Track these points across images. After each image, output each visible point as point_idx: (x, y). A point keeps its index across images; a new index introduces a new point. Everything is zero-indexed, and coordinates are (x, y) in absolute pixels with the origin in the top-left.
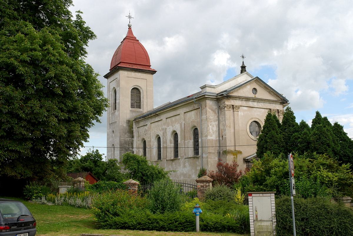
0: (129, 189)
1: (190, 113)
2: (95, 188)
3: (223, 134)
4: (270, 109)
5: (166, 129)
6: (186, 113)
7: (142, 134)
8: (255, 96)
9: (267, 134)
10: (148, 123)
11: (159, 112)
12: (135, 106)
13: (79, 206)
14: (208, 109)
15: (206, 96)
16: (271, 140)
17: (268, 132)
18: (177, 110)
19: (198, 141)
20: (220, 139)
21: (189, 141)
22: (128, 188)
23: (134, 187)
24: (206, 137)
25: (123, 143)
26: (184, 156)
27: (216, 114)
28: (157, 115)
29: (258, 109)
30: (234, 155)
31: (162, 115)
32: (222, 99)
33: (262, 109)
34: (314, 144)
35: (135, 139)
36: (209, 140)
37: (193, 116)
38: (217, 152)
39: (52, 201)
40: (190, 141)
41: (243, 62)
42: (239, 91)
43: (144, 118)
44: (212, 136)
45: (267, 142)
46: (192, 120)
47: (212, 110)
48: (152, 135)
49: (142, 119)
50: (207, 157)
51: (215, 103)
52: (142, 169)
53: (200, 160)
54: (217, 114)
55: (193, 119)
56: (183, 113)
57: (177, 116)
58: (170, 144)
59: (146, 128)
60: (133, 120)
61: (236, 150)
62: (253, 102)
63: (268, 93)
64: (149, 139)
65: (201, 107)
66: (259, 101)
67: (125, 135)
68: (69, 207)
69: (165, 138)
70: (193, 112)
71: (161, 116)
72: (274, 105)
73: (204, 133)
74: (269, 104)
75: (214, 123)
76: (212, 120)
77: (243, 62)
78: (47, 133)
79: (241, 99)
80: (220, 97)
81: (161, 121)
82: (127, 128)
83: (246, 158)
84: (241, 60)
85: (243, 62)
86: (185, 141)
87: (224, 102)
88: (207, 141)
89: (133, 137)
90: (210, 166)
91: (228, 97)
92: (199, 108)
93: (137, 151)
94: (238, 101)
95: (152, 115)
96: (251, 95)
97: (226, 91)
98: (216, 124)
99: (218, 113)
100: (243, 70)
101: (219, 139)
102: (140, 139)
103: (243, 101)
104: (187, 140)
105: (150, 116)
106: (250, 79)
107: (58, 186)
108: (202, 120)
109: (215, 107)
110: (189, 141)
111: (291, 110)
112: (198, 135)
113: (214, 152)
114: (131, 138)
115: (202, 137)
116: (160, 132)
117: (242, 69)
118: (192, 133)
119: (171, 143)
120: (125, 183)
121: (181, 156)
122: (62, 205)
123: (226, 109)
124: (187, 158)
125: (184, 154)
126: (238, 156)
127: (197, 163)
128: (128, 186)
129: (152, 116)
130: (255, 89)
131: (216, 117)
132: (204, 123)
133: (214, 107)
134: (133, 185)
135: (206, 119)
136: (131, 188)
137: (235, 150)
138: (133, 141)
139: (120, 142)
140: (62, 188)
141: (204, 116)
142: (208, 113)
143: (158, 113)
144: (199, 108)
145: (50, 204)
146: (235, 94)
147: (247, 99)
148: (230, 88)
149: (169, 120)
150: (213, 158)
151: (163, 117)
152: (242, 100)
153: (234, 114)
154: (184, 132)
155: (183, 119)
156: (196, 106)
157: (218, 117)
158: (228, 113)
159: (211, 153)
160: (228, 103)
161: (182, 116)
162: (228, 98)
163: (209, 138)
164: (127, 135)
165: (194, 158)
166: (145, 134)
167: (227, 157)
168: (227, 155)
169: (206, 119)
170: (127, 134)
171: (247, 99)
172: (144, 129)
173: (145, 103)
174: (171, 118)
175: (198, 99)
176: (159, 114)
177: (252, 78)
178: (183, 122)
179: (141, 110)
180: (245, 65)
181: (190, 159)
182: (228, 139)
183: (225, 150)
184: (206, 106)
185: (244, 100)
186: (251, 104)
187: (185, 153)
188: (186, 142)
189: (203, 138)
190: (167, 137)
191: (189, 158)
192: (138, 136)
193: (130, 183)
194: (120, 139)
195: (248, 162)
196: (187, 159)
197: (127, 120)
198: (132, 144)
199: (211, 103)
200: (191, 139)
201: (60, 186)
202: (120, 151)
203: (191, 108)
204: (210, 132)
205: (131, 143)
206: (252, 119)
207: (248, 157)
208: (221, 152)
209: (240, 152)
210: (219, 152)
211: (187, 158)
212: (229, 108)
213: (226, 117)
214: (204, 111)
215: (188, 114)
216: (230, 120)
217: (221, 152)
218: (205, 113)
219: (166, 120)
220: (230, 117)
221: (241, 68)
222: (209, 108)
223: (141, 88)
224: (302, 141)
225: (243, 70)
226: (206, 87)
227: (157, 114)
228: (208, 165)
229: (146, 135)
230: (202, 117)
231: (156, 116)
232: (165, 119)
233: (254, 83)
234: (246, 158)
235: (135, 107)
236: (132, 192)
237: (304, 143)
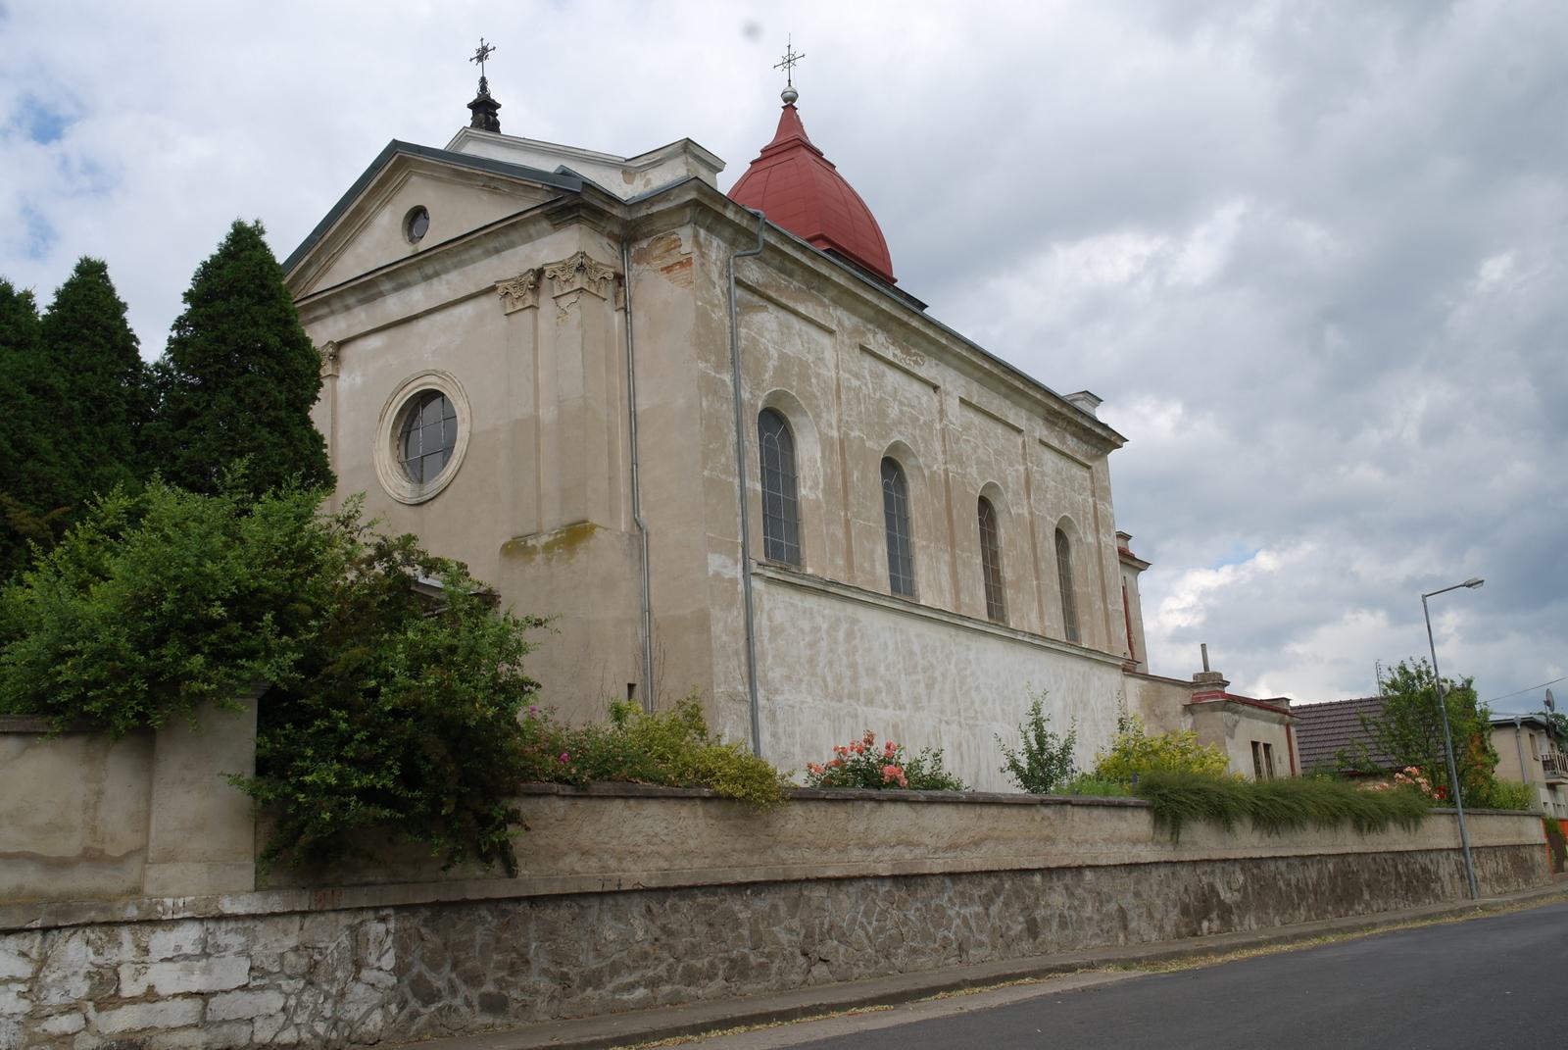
62: (404, 294)
74: (494, 260)
84: (782, 75)
85: (483, 81)
152: (348, 308)
185: (351, 300)
227: (753, 238)
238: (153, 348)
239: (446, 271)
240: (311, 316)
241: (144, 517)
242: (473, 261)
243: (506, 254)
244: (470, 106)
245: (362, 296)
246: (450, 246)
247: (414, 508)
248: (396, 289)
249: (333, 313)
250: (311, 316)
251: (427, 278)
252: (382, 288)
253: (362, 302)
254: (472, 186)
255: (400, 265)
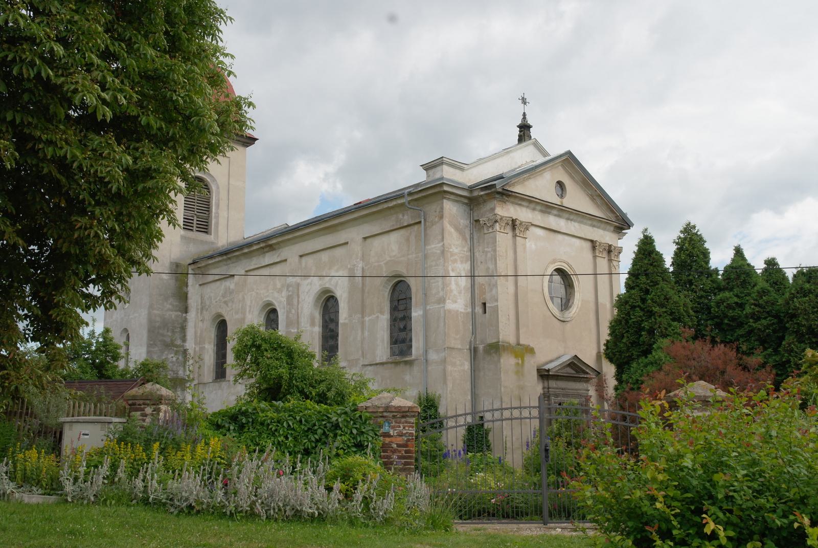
0: (382, 431)
1: (385, 239)
2: (232, 428)
3: (488, 296)
4: (592, 241)
5: (298, 285)
6: (369, 241)
7: (214, 302)
8: (562, 202)
9: (647, 292)
10: (238, 269)
11: (280, 239)
12: (195, 225)
13: (190, 507)
14: (448, 226)
15: (446, 188)
16: (664, 310)
17: (650, 286)
18: (338, 231)
19: (407, 318)
20: (476, 311)
21: (378, 317)
22: (381, 427)
23: (406, 422)
24: (439, 304)
25: (157, 324)
26: (361, 359)
27: (466, 241)
28: (271, 248)
29: (566, 238)
30: (516, 357)
31: (287, 248)
32: (485, 201)
33: (574, 240)
34: (807, 320)
35: (192, 316)
36: (450, 311)
37: (395, 247)
38: (468, 347)
39: (38, 483)
40: (381, 317)
41: (524, 113)
42: (526, 183)
43: (225, 257)
44: (456, 302)
45: (650, 314)
46: (388, 259)
47: (457, 229)
48: (248, 303)
49: (217, 260)
50: (444, 361)
51: (465, 211)
52: (304, 378)
53: (416, 369)
54: (469, 241)
55: (394, 254)
56: (359, 238)
57: (338, 248)
58: (309, 328)
59: (230, 284)
60: (190, 264)
61: (522, 342)
62: (557, 219)
63: (588, 199)
64: (239, 316)
65: (425, 220)
66: (572, 217)
67: (165, 304)
68: (145, 515)
69: (293, 311)
70: (394, 237)
71: (281, 250)
72: (601, 232)
73: (434, 291)
74: (590, 229)
75: (460, 266)
76: (456, 257)
77: (524, 113)
78: (44, 159)
79: (532, 206)
80: (482, 193)
81: (283, 264)
82: (172, 283)
83: (547, 363)
84: (520, 108)
85: (524, 114)
86: (363, 317)
87: (493, 209)
88: (442, 315)
89: (186, 310)
90: (450, 385)
91: (505, 195)
92: (420, 222)
93: (197, 349)
94: (524, 209)
95: (255, 247)
96: (551, 196)
97: (500, 177)
98: (466, 268)
99: (472, 238)
100: (524, 134)
101: (473, 313)
102: (208, 316)
103: (537, 213)
104: (369, 316)
105: (246, 250)
106: (541, 159)
107: (57, 417)
108: (426, 257)
109: (464, 222)
110: (378, 317)
111: (699, 233)
112: (411, 298)
113: (459, 347)
114: (180, 311)
115: (425, 302)
116: (276, 295)
117: (520, 131)
118: (387, 293)
119: (313, 324)
120: (366, 408)
121: (349, 361)
122: (100, 500)
123: (497, 226)
124: (371, 365)
125: (360, 352)
126: (525, 359)
127: (407, 378)
128: (380, 420)
129: (252, 249)
130: (560, 184)
131: (465, 249)
132: (434, 263)
133: (462, 221)
134: (403, 417)
135: (443, 252)
136: (393, 428)
137: (518, 344)
138: (185, 320)
139: (151, 321)
140: (75, 425)
141: (433, 246)
142: (446, 235)
143: (274, 241)
144: (420, 222)
145: (34, 498)
146: (518, 189)
147: (547, 207)
148: (510, 171)
149: (309, 261)
150: (458, 362)
151: (291, 252)
152: (534, 209)
153: (515, 244)
154: (363, 291)
155: (360, 255)
156: (406, 219)
157: (472, 250)
158: (503, 238)
159: (453, 348)
160: (506, 211)
161: (356, 247)
162: (504, 197)
163: (450, 305)
164: (171, 304)
165: (396, 363)
166: (226, 303)
167: (502, 361)
168: (500, 356)
169: (443, 252)
170: (171, 300)
171: (547, 207)
172: (223, 287)
173: (222, 222)
174: (315, 256)
175: (416, 197)
176: (278, 243)
177: (545, 156)
178: (360, 265)
179: (211, 238)
180: (530, 122)
181: (380, 368)
182: (501, 311)
183: (494, 341)
184: (441, 217)
185: (539, 208)
186: (553, 221)
187: (363, 353)
188: (367, 319)
189: (428, 307)
190: (300, 309)
191: (377, 364)
192: (199, 307)
193: (387, 409)
194: (149, 314)
195: (548, 380)
196: (370, 368)
197: (172, 260)
198: (183, 329)
199: (455, 208)
200: (382, 313)
201: (69, 419)
202: (148, 347)
203: (387, 225)
204: (451, 291)
205: (180, 326)
206: (554, 261)
207: (551, 361)
208: (481, 347)
209: (530, 350)
210: (474, 347)
211: (371, 365)
212: (504, 225)
213: (498, 249)
214: (435, 229)
215: (377, 243)
216: (506, 258)
217: (481, 347)
218: (440, 237)
219: (300, 262)
220: (506, 251)
221: (518, 129)
222: (451, 223)
223: (214, 180)
224: (758, 311)
225: (524, 134)
226: (442, 163)
227: (270, 246)
228: (445, 382)
229: (230, 304)
230: (427, 247)
231: (265, 250)
232: (297, 258)
233: (560, 167)
234: (547, 363)
235: (195, 229)
236: (399, 445)
237: (765, 318)
238: (791, 281)
239: (575, 221)
240: (520, 202)
241: (814, 329)
242: (585, 224)
243: (595, 229)
244: (518, 126)
245: (544, 209)
246: (588, 216)
247: (560, 322)
248: (555, 215)
249: (527, 207)
250: (520, 202)
251: (568, 219)
252: (552, 212)
253: (542, 211)
254: (585, 191)
255: (525, 197)
